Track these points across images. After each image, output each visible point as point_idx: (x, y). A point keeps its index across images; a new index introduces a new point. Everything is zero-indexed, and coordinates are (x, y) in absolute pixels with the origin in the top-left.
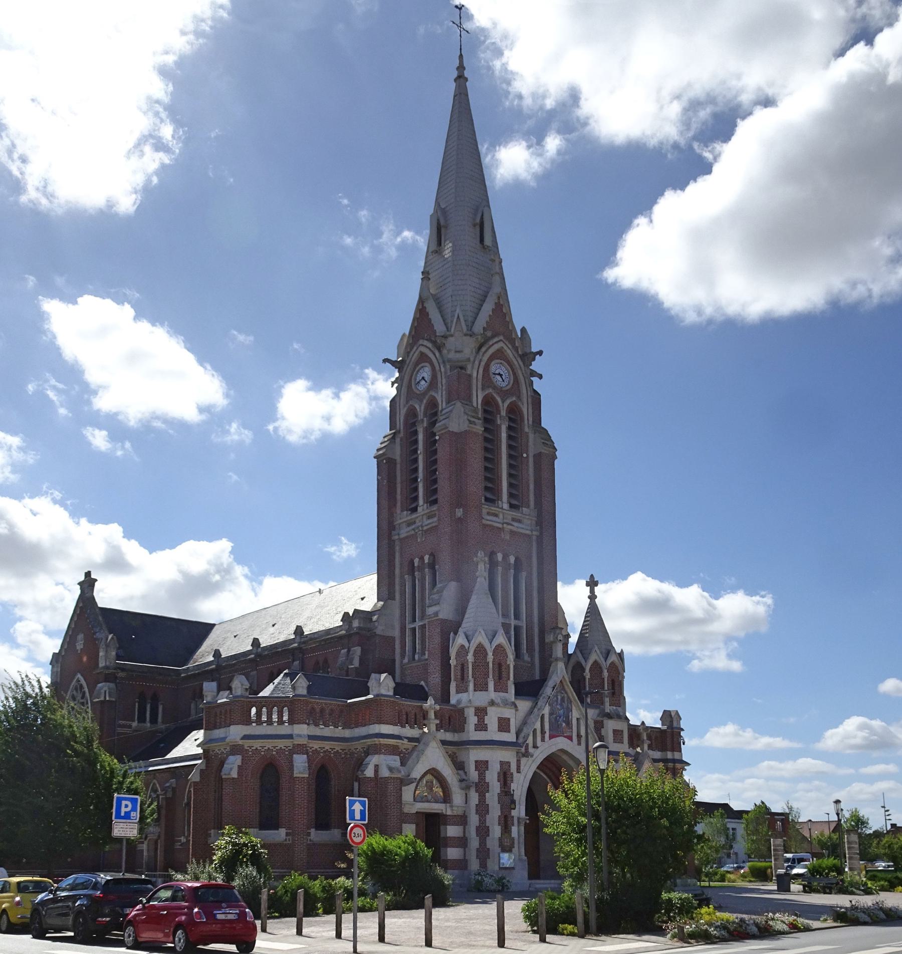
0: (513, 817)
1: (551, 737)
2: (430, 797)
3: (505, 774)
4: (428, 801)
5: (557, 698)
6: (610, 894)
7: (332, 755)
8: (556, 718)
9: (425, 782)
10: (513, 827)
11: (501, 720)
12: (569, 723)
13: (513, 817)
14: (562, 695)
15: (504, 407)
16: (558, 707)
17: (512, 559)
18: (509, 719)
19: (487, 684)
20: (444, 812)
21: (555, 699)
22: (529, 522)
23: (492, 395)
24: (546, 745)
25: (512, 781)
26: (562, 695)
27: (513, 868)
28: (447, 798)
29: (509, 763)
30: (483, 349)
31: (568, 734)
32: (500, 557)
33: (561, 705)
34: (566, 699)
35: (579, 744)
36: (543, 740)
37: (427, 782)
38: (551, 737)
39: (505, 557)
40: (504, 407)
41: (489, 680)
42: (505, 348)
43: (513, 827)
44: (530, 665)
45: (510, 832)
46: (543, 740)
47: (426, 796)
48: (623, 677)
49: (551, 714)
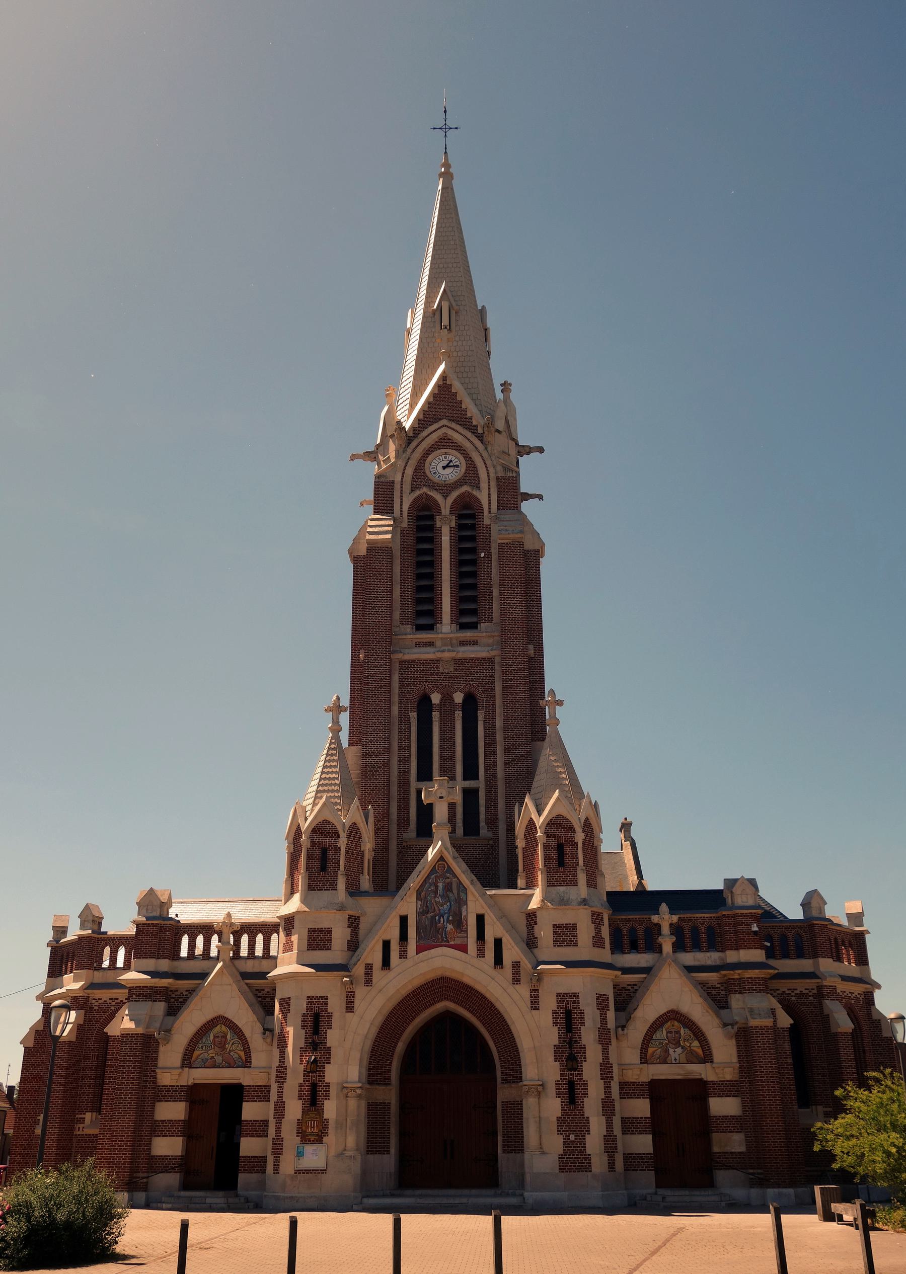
0: (328, 1085)
1: (419, 950)
2: (219, 1059)
3: (568, 1014)
4: (214, 1066)
5: (437, 887)
6: (57, 1224)
7: (853, 1002)
8: (433, 918)
9: (212, 1037)
10: (326, 1102)
11: (571, 928)
12: (459, 924)
13: (328, 1085)
14: (448, 880)
15: (445, 505)
16: (440, 900)
17: (459, 698)
18: (329, 930)
19: (575, 876)
20: (703, 1076)
21: (433, 888)
22: (490, 641)
23: (428, 495)
24: (408, 963)
25: (330, 1026)
26: (448, 880)
27: (324, 1171)
28: (707, 1057)
29: (324, 1000)
30: (414, 444)
31: (458, 941)
32: (436, 698)
33: (445, 896)
34: (454, 886)
35: (481, 953)
36: (403, 955)
37: (215, 1037)
38: (419, 950)
39: (447, 698)
40: (445, 505)
41: (579, 869)
42: (450, 432)
43: (326, 1102)
44: (491, 842)
45: (320, 1112)
46: (403, 955)
47: (212, 1058)
48: (601, 841)
49: (421, 913)
